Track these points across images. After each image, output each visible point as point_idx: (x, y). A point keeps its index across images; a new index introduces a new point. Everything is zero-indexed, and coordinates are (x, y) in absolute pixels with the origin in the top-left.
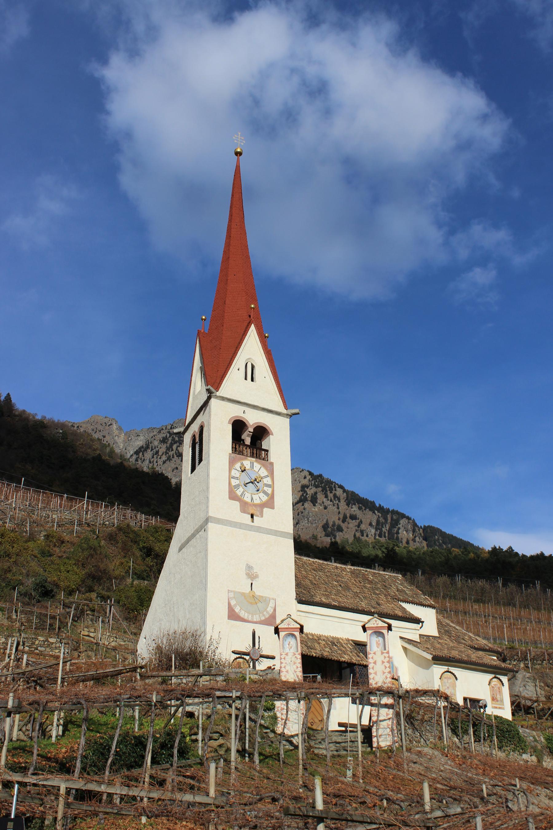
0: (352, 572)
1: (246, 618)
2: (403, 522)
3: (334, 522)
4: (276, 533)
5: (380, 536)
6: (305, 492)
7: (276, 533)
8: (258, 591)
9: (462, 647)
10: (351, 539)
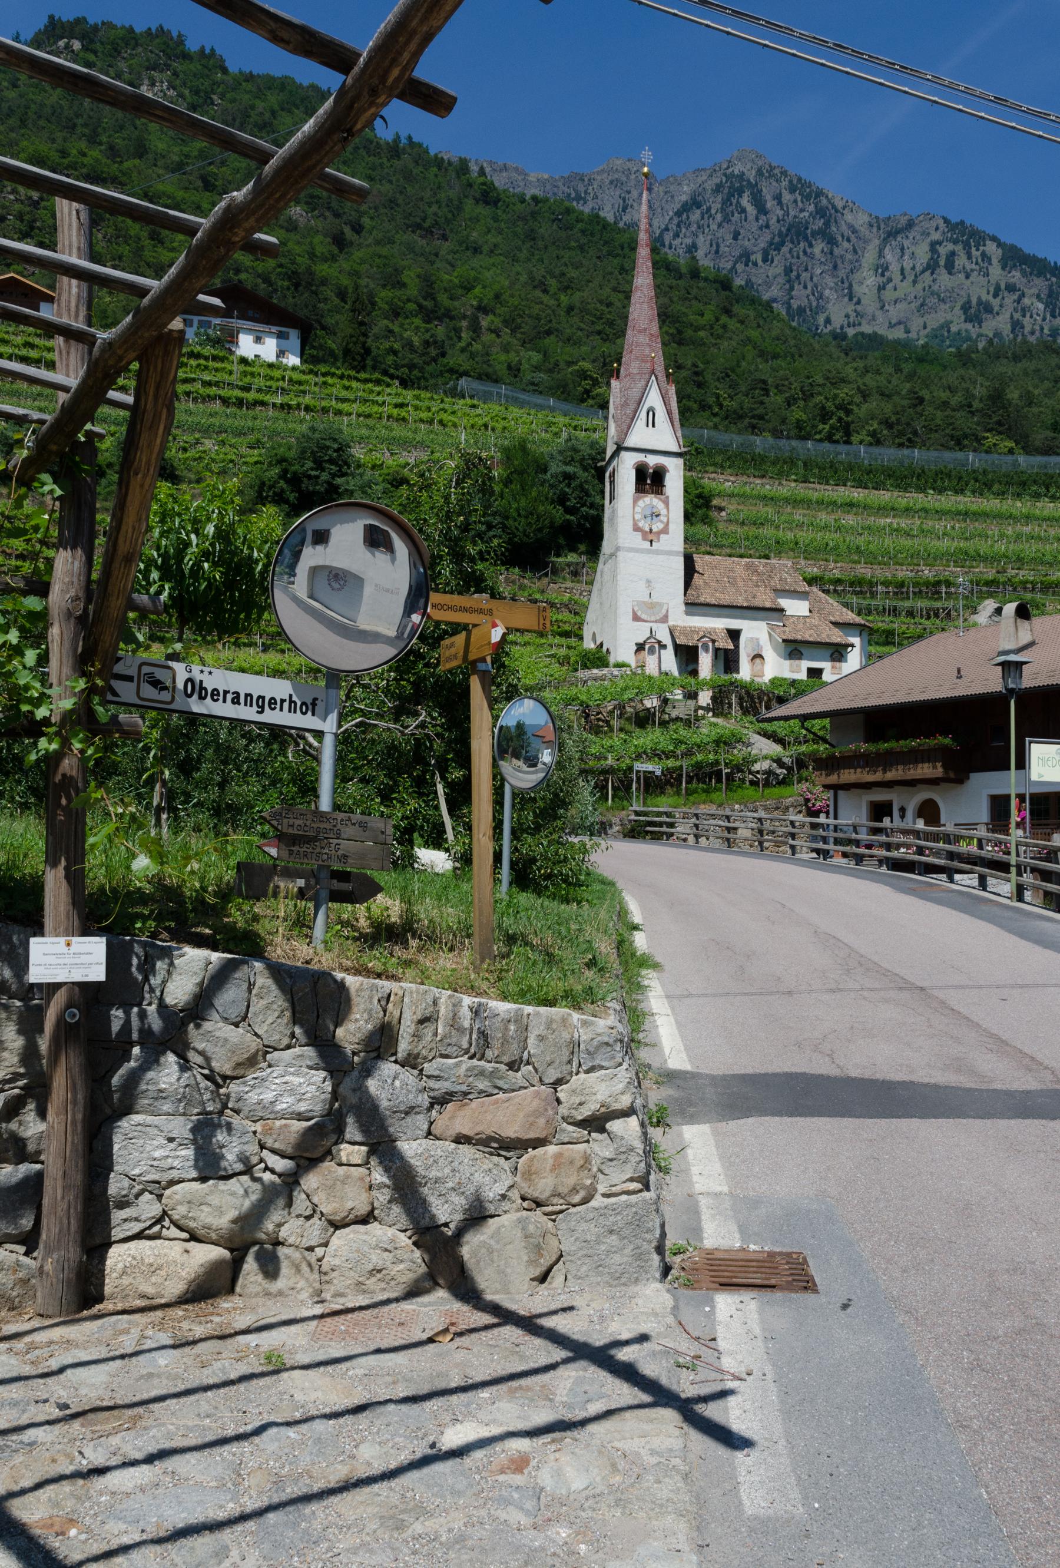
3: (979, 298)
4: (669, 553)
7: (669, 553)
8: (655, 598)
10: (1006, 329)
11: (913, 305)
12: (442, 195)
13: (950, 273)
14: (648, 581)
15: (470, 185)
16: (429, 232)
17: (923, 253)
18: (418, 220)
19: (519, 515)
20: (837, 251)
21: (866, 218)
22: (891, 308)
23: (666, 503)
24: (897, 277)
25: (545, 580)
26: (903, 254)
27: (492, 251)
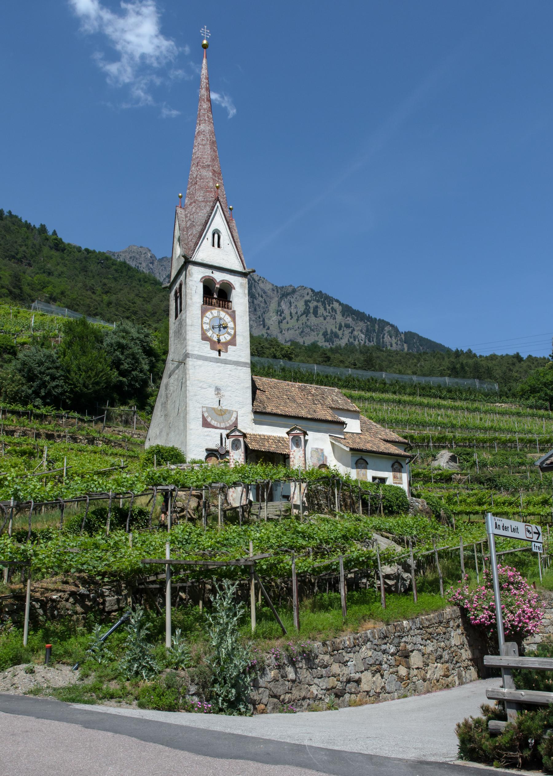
0: (299, 388)
1: (215, 425)
2: (387, 328)
3: (332, 330)
4: (237, 363)
5: (369, 341)
6: (308, 305)
7: (237, 363)
8: (225, 405)
9: (377, 441)
11: (297, 332)
12: (29, 243)
13: (316, 317)
14: (218, 389)
15: (47, 239)
16: (20, 261)
17: (301, 307)
18: (13, 254)
19: (79, 369)
20: (256, 302)
21: (271, 287)
22: (286, 333)
23: (233, 316)
24: (288, 318)
25: (101, 425)
26: (291, 306)
27: (60, 275)
